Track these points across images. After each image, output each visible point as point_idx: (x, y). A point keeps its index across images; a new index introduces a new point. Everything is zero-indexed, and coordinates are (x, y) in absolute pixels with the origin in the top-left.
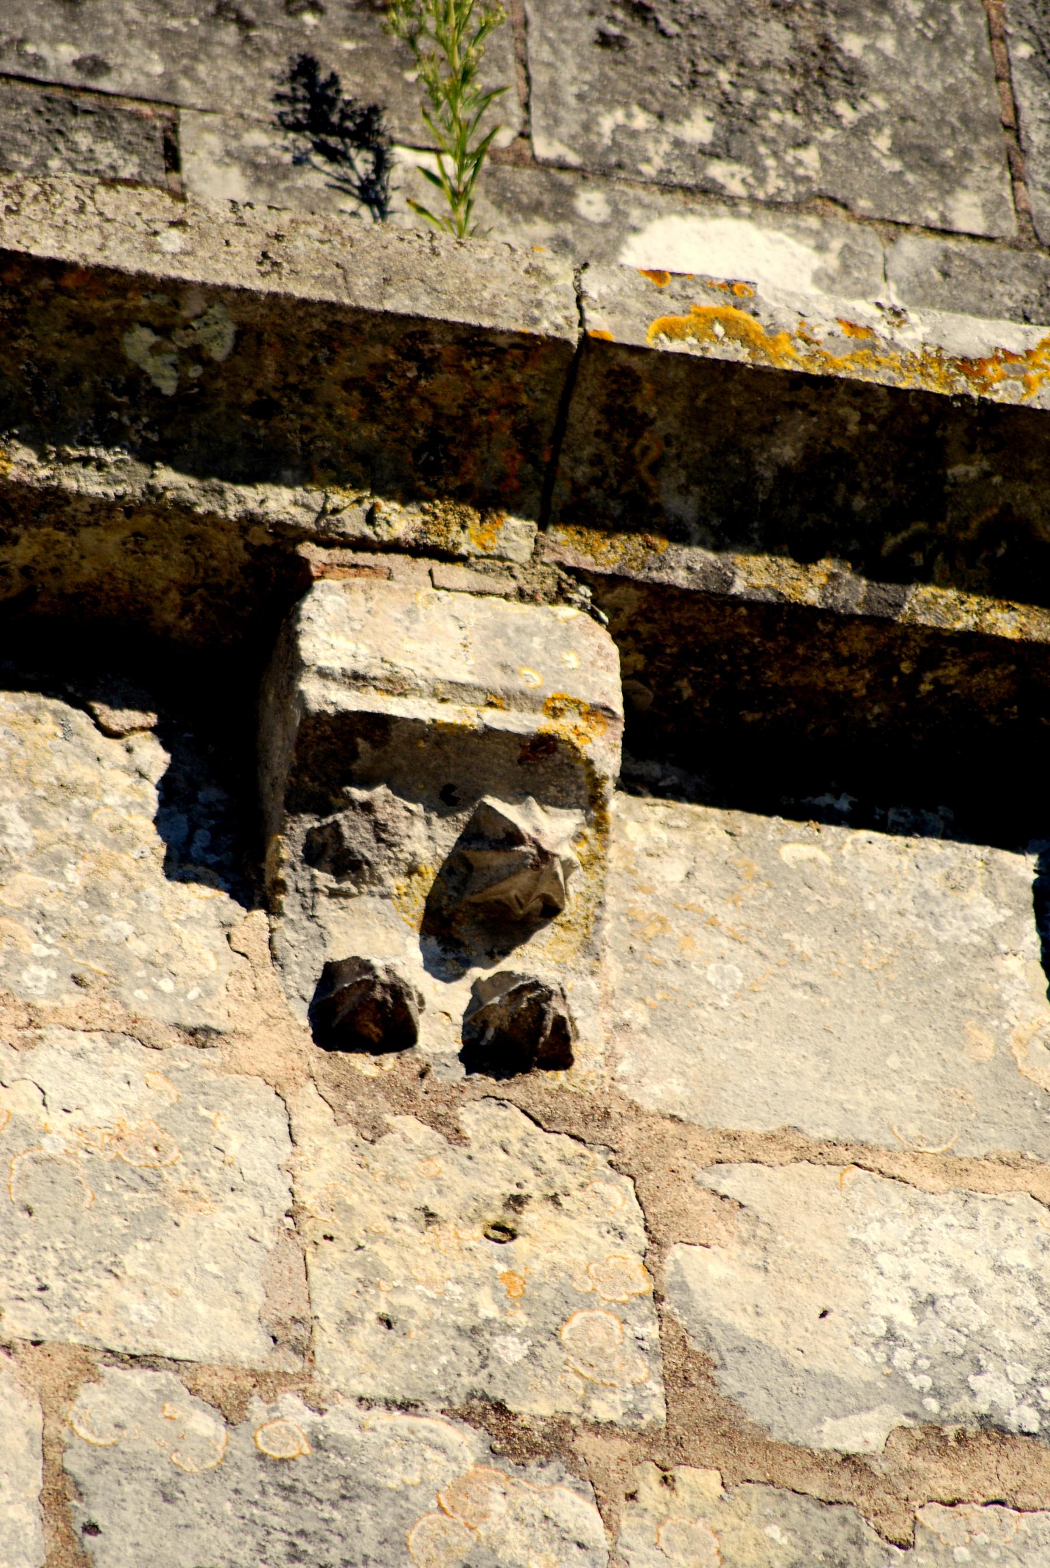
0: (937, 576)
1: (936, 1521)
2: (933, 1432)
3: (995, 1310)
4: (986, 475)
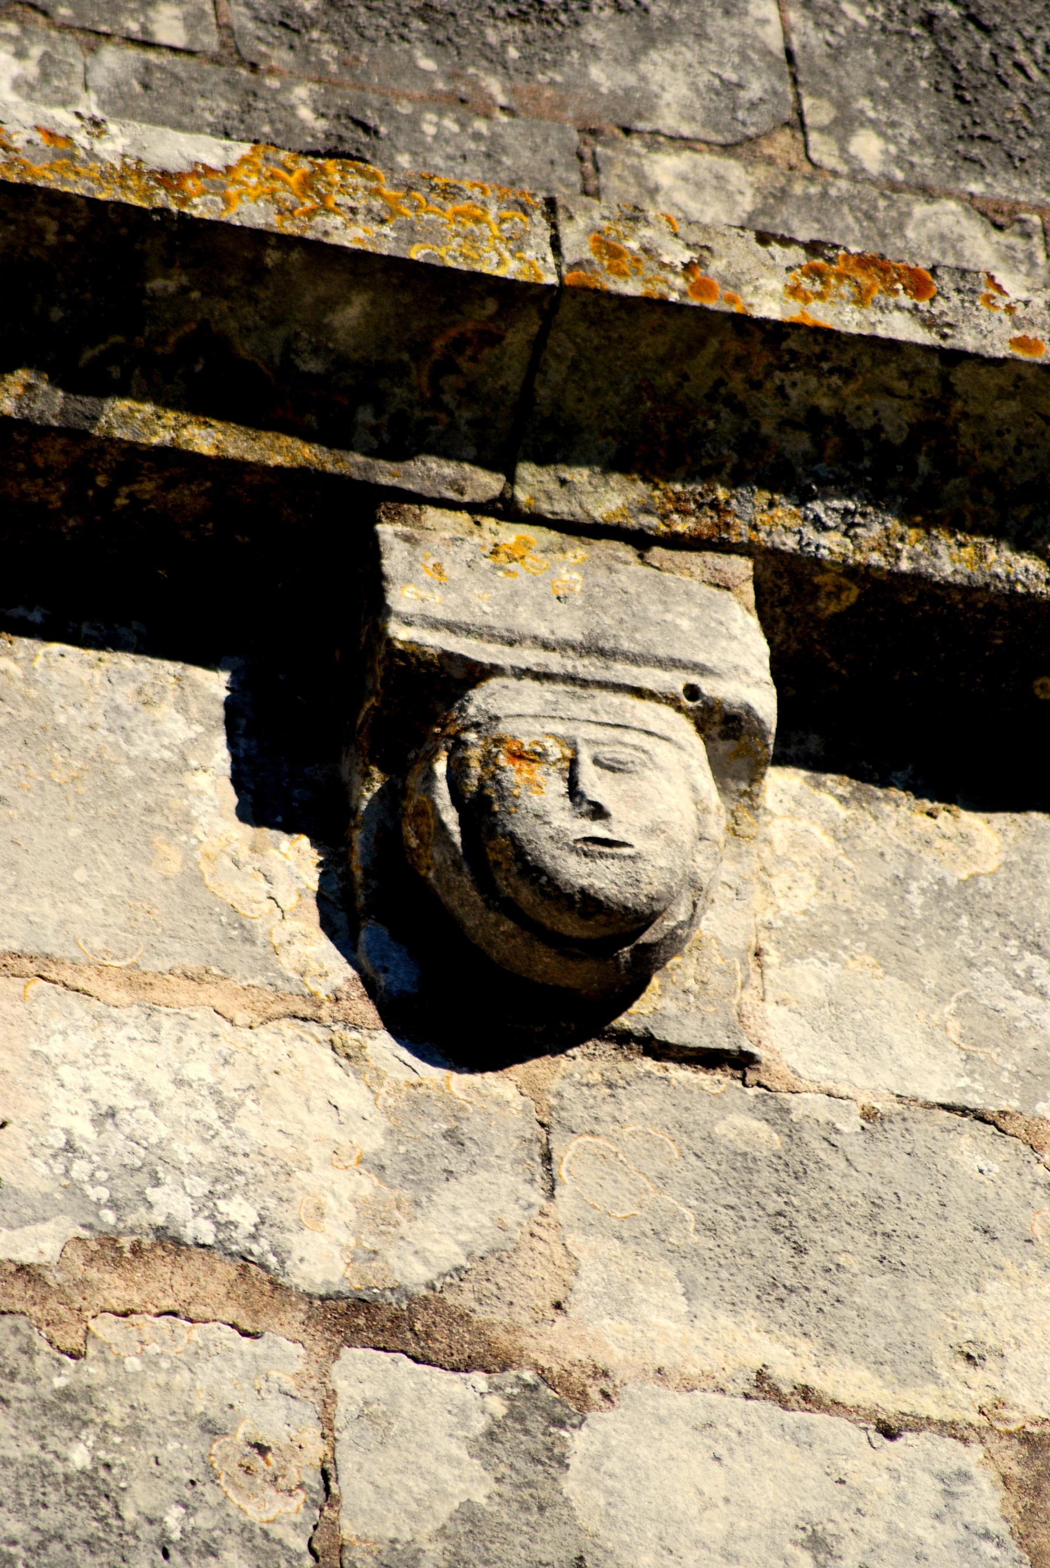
0: (134, 390)
1: (108, 1331)
2: (109, 1243)
3: (175, 1123)
4: (184, 290)
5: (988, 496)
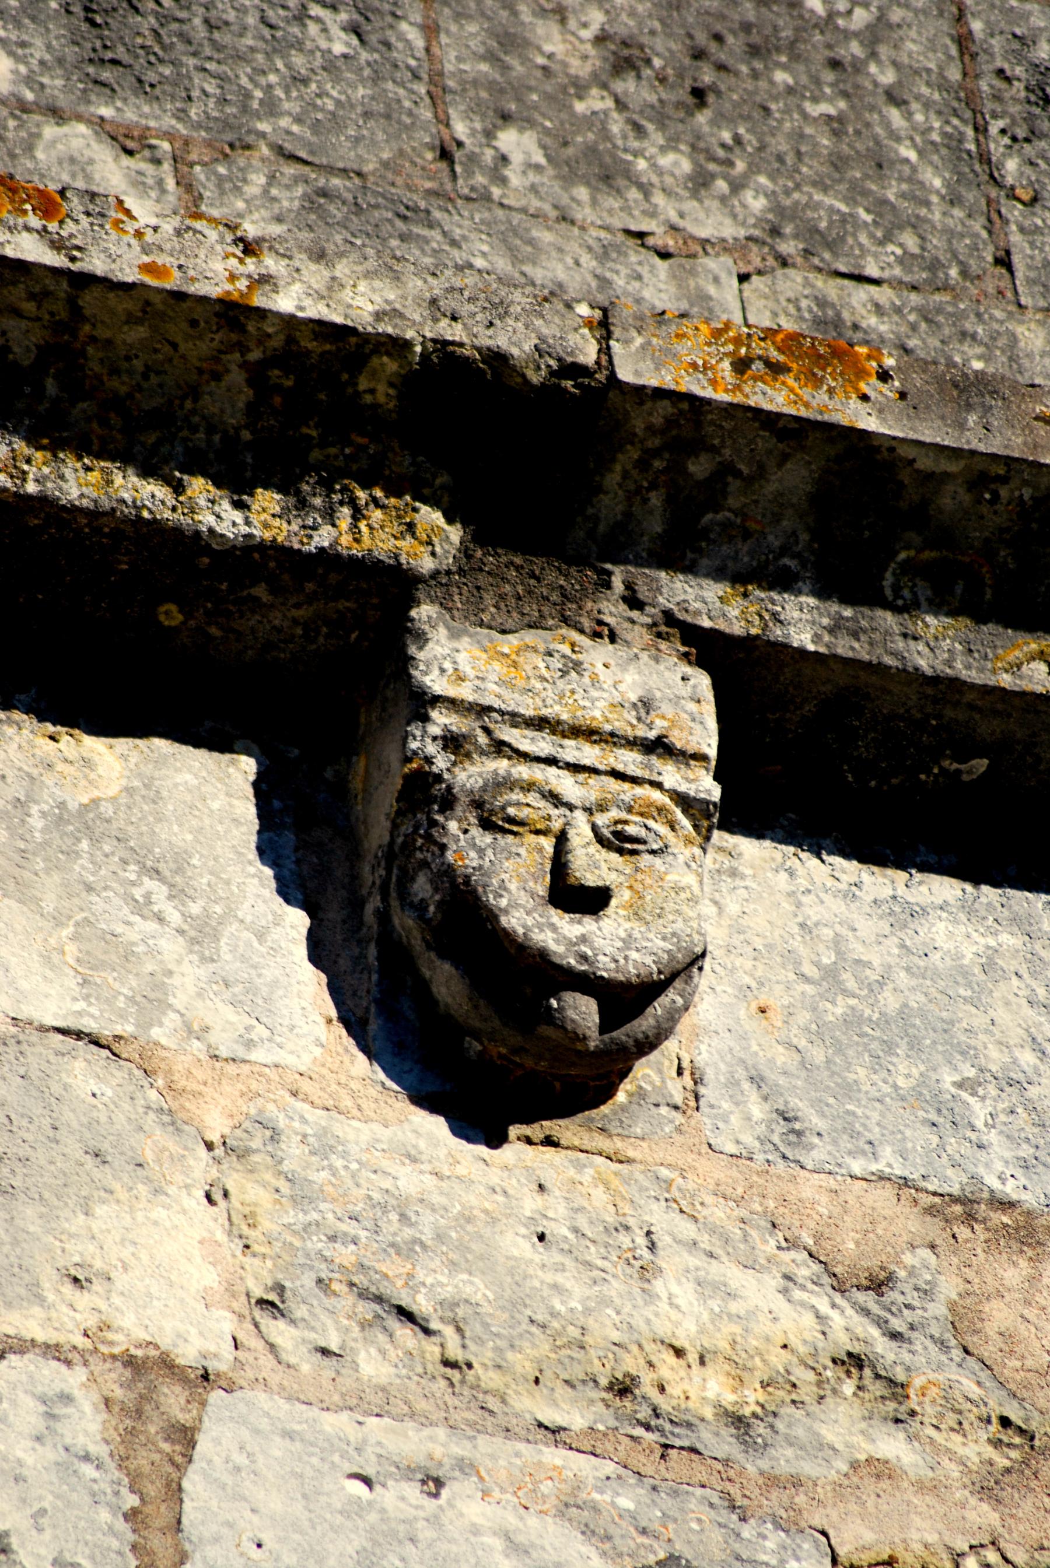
5: (115, 420)
